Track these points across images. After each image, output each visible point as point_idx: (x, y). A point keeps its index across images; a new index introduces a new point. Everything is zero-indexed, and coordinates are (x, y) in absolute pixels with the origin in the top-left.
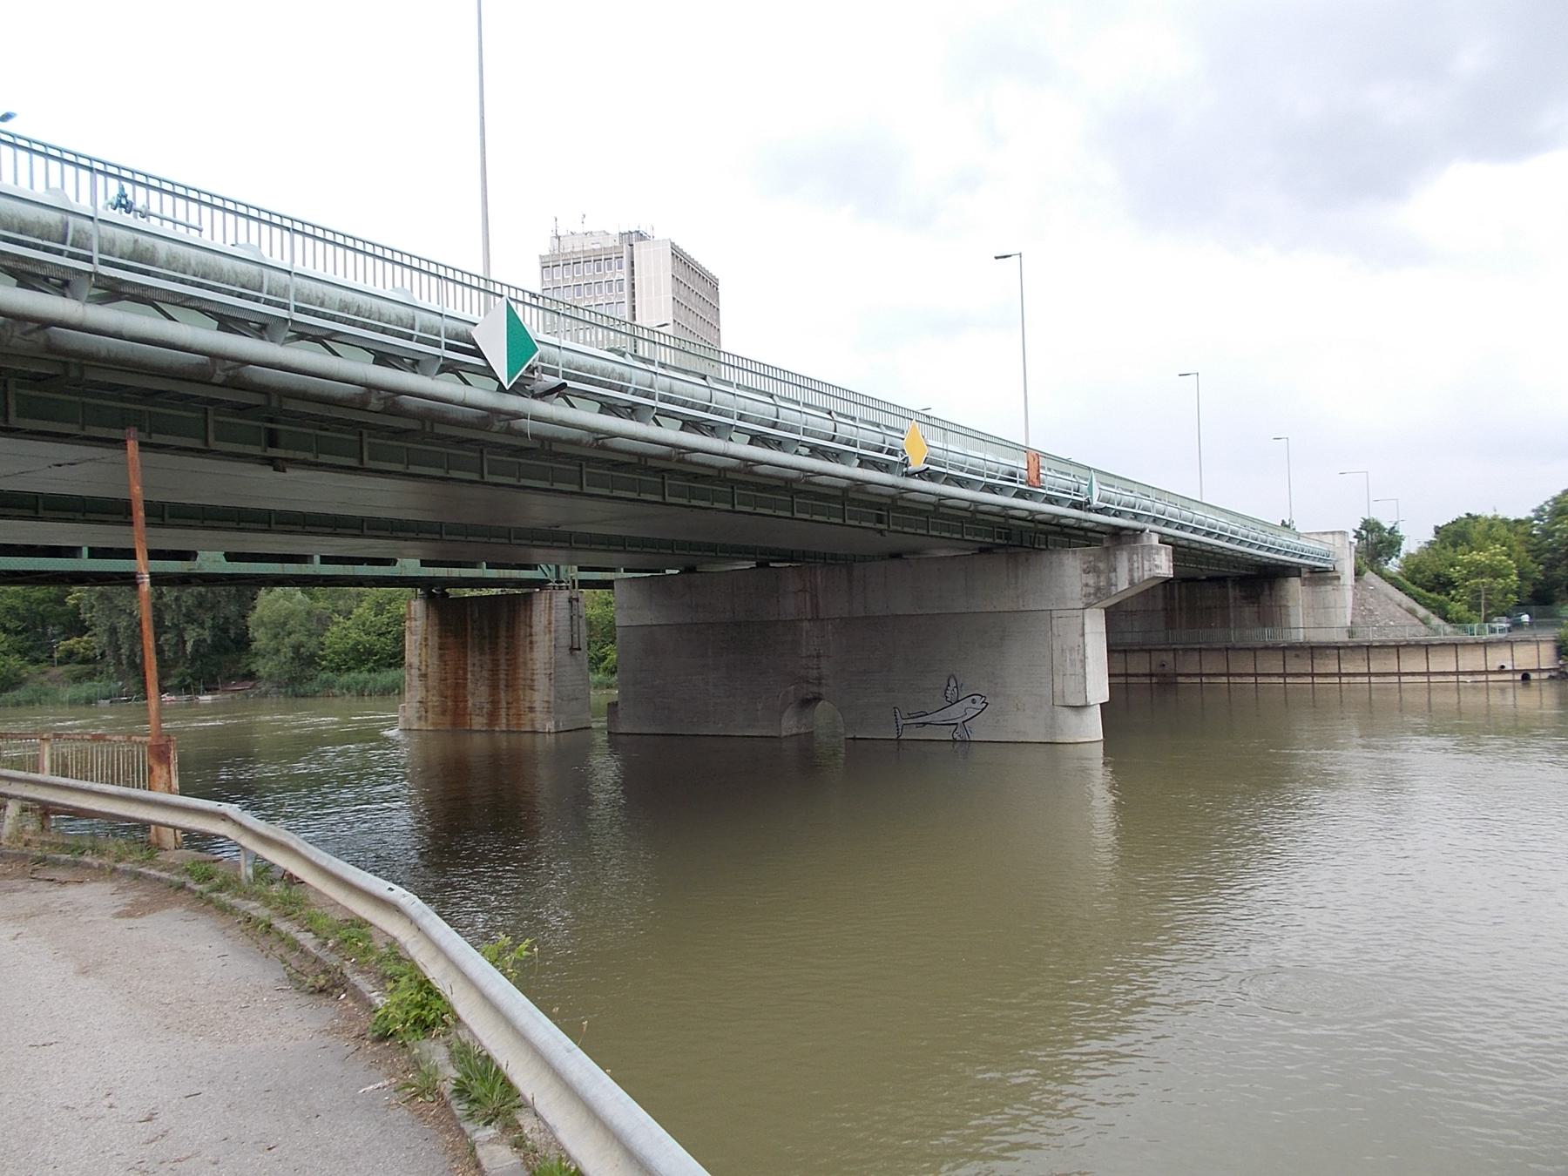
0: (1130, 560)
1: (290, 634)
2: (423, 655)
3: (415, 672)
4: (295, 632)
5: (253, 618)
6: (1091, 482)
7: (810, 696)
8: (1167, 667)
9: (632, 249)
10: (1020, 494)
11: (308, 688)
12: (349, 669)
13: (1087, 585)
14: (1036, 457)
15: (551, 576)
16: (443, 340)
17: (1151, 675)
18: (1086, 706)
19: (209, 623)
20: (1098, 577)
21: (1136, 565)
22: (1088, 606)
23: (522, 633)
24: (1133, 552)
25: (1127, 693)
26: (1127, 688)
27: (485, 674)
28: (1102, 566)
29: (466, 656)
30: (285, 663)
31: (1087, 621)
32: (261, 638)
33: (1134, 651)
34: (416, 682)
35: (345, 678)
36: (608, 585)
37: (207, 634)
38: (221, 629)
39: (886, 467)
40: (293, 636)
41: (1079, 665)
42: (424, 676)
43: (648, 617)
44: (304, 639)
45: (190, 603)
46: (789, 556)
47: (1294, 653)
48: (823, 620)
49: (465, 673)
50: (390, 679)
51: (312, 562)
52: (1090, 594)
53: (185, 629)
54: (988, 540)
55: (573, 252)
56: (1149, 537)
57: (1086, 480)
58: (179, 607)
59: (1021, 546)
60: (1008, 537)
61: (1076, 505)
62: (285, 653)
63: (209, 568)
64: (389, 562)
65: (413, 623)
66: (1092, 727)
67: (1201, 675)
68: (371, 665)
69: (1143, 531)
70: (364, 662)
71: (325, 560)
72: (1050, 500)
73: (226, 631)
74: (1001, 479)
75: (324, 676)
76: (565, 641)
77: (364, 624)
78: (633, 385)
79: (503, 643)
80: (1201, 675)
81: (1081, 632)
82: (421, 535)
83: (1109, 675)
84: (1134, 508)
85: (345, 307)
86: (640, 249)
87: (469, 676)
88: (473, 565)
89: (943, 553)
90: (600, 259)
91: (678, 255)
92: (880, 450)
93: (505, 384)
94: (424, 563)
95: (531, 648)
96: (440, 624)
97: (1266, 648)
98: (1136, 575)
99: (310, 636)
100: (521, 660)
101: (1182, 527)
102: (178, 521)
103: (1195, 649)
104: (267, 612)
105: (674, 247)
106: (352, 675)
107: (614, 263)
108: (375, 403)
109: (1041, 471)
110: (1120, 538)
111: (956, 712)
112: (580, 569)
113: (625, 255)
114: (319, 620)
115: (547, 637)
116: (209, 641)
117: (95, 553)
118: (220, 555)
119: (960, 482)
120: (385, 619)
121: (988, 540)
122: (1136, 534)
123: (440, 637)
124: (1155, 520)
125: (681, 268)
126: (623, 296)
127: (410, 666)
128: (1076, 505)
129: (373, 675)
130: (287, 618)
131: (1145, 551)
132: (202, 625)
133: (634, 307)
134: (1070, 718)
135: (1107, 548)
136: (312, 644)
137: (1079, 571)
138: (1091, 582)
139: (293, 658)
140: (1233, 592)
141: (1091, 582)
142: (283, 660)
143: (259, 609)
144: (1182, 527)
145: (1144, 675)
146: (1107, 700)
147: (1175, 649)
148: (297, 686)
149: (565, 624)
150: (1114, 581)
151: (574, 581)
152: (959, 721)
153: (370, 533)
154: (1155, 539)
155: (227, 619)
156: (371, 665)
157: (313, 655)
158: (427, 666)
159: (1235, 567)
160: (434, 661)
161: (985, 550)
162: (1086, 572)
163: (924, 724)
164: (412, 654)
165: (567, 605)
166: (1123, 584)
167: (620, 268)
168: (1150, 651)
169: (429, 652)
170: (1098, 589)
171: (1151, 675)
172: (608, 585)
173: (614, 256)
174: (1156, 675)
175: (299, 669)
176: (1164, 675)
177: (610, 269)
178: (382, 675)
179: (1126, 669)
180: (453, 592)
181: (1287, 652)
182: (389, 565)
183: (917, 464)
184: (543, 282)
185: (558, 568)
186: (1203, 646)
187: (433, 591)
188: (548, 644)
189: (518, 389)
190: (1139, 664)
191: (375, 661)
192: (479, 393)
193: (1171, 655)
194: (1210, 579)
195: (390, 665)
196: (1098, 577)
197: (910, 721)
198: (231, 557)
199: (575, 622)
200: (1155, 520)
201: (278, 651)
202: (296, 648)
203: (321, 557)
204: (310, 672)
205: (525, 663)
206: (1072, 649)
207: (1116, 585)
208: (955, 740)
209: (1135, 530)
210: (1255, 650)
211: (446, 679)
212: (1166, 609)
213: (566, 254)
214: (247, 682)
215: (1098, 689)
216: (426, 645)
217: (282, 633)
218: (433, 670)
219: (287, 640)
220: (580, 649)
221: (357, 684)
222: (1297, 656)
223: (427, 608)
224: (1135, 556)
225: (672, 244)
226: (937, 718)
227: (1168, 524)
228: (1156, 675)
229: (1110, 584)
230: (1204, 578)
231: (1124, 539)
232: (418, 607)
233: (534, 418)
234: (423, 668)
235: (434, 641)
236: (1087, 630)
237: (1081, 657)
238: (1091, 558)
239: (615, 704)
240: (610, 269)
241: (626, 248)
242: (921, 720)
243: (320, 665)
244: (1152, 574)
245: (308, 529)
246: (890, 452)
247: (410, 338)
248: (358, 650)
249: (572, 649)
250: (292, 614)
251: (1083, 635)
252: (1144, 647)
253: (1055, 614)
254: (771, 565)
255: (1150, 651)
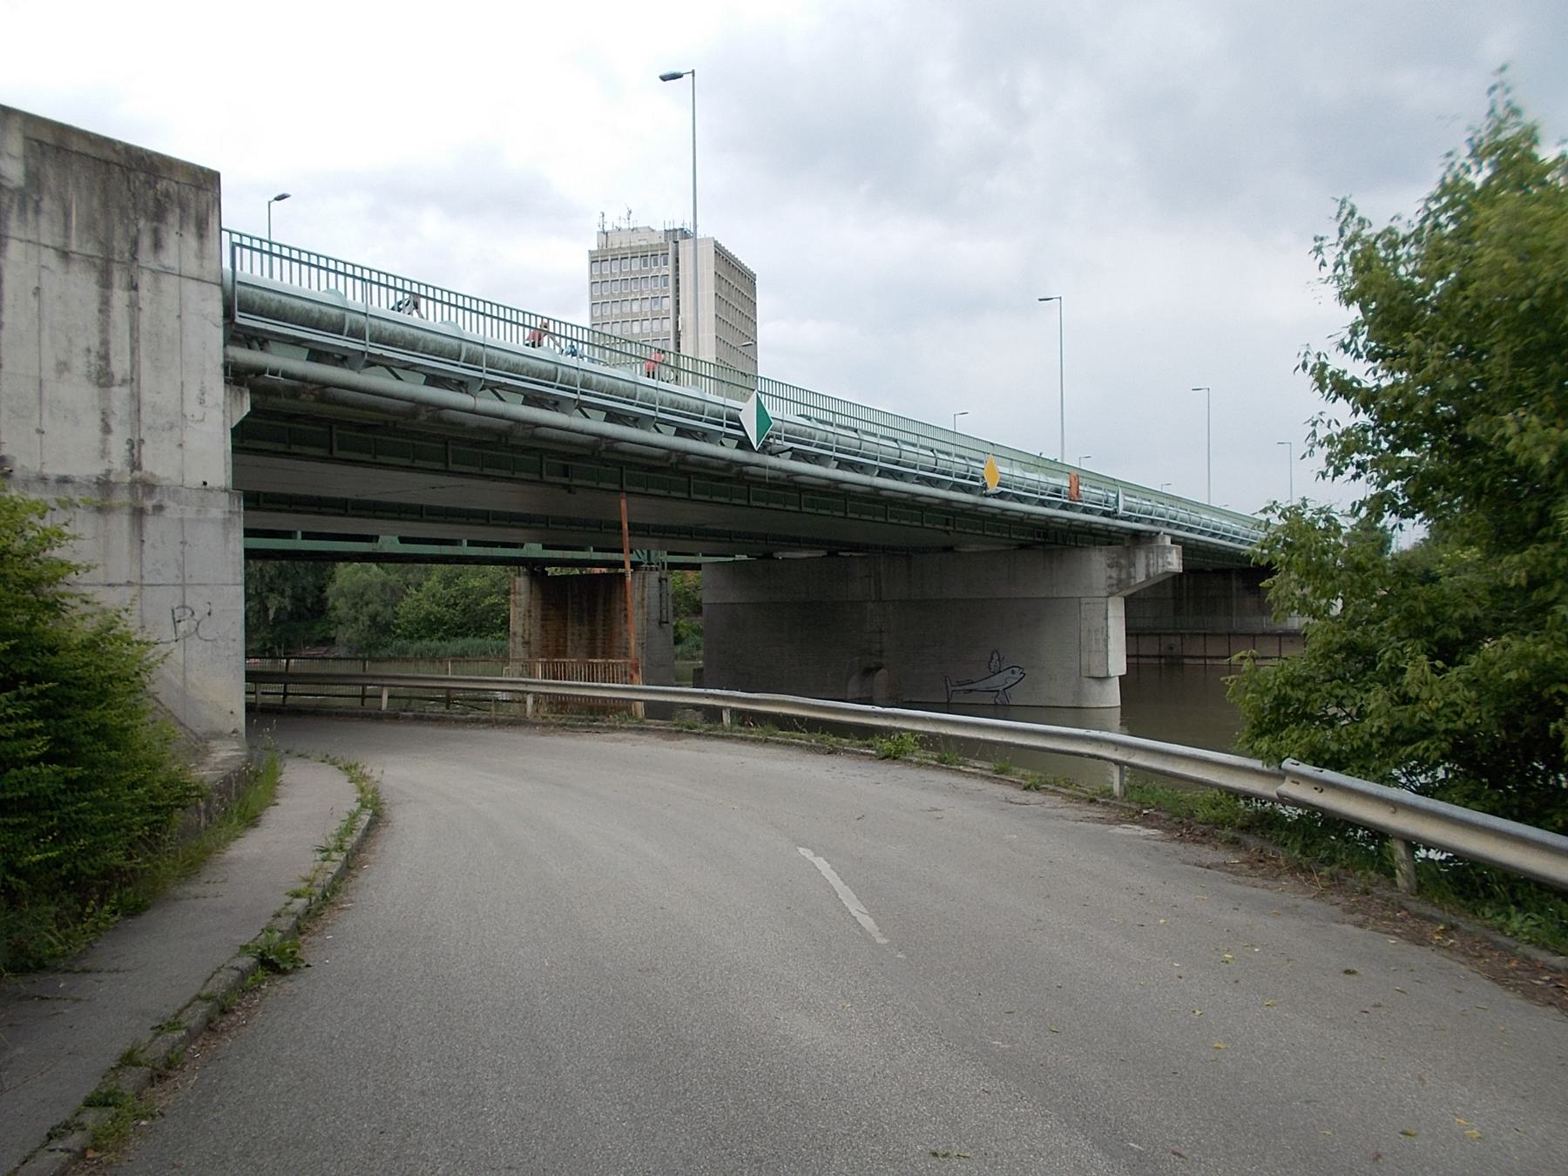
0: (1147, 557)
1: (367, 604)
2: (527, 627)
3: (519, 640)
4: (371, 602)
5: (331, 590)
6: (1118, 496)
7: (873, 666)
8: (1175, 650)
9: (677, 246)
10: (1064, 507)
11: (384, 653)
12: (421, 638)
13: (1110, 577)
14: (1077, 476)
15: (644, 558)
16: (725, 422)
17: (1160, 657)
18: (1108, 677)
19: (289, 592)
20: (1120, 571)
21: (1151, 562)
22: (1111, 594)
23: (618, 607)
24: (1150, 551)
25: (1138, 673)
26: (1138, 668)
27: (584, 642)
28: (1123, 561)
29: (566, 626)
30: (363, 631)
31: (1110, 608)
32: (341, 607)
33: (1145, 635)
34: (520, 648)
35: (418, 645)
36: (697, 567)
37: (287, 602)
38: (298, 599)
39: (968, 490)
40: (370, 606)
41: (1102, 643)
42: (527, 643)
43: (732, 597)
44: (381, 609)
45: (272, 573)
46: (856, 547)
47: (1288, 639)
48: (885, 601)
49: (566, 641)
50: (459, 647)
51: (296, 538)
52: (1113, 585)
53: (267, 597)
54: (1029, 538)
55: (620, 248)
56: (1163, 538)
57: (1113, 492)
58: (262, 577)
59: (1056, 543)
60: (1046, 536)
61: (1105, 514)
62: (363, 621)
63: (386, 550)
64: (520, 545)
65: (518, 597)
66: (1112, 695)
67: (1205, 657)
68: (440, 634)
69: (1158, 533)
70: (434, 631)
71: (471, 543)
72: (1086, 511)
73: (303, 600)
74: (1049, 495)
75: (399, 643)
76: (655, 615)
77: (434, 596)
78: (816, 441)
79: (600, 617)
80: (1205, 657)
81: (1104, 615)
82: (533, 525)
83: (1127, 656)
84: (1150, 514)
85: (672, 404)
86: (686, 248)
87: (569, 643)
88: (582, 549)
89: (973, 548)
90: (647, 255)
91: (721, 254)
92: (964, 477)
93: (755, 445)
94: (545, 547)
95: (626, 622)
96: (542, 599)
97: (1264, 634)
98: (1151, 570)
99: (385, 606)
100: (617, 630)
101: (1190, 530)
102: (271, 506)
103: (1198, 634)
104: (347, 584)
105: (717, 245)
106: (424, 642)
107: (660, 260)
108: (674, 459)
109: (1081, 488)
110: (1139, 540)
111: (997, 681)
112: (669, 554)
113: (670, 251)
114: (393, 591)
115: (641, 611)
116: (289, 609)
117: (307, 536)
118: (396, 539)
119: (1020, 499)
120: (453, 590)
121: (1029, 538)
122: (1151, 537)
123: (542, 610)
124: (1168, 524)
125: (724, 266)
126: (668, 291)
127: (514, 634)
128: (1105, 514)
129: (443, 643)
130: (365, 588)
131: (1160, 550)
132: (282, 594)
133: (678, 301)
134: (1095, 687)
135: (1128, 547)
136: (388, 613)
137: (1104, 565)
138: (1114, 575)
139: (370, 626)
140: (1236, 584)
141: (1114, 575)
142: (362, 627)
143: (339, 581)
144: (1190, 530)
145: (1154, 656)
146: (1124, 673)
147: (1182, 634)
148: (373, 652)
149: (655, 601)
150: (1133, 574)
151: (663, 564)
152: (1001, 689)
153: (353, 512)
154: (1168, 540)
155: (304, 589)
156: (440, 634)
157: (388, 624)
158: (530, 635)
159: (1238, 561)
160: (537, 630)
161: (1023, 547)
162: (1110, 566)
163: (971, 690)
164: (516, 625)
165: (656, 583)
166: (1140, 577)
167: (666, 264)
168: (1159, 635)
169: (532, 622)
170: (1120, 581)
171: (1160, 657)
172: (697, 567)
173: (660, 252)
174: (1165, 657)
175: (375, 637)
176: (1172, 657)
177: (656, 264)
178: (452, 643)
179: (1138, 650)
180: (550, 571)
181: (1283, 639)
182: (371, 541)
183: (993, 488)
184: (591, 276)
185: (649, 552)
186: (1208, 632)
187: (534, 568)
188: (641, 618)
189: (765, 449)
190: (1149, 647)
191: (445, 631)
192: (729, 451)
193: (1179, 639)
194: (1216, 571)
195: (456, 635)
196: (1120, 571)
197: (958, 688)
198: (403, 540)
199: (664, 599)
200: (1168, 524)
201: (356, 619)
202: (373, 618)
203: (468, 541)
204: (384, 639)
205: (621, 635)
206: (1096, 630)
207: (1134, 578)
208: (996, 704)
209: (1151, 532)
210: (1254, 635)
211: (547, 647)
212: (1175, 598)
213: (614, 250)
214: (319, 648)
215: (1118, 665)
216: (530, 616)
217: (360, 603)
218: (536, 638)
219: (365, 609)
220: (667, 623)
221: (429, 650)
222: (1291, 641)
223: (531, 584)
224: (1151, 555)
225: (716, 242)
226: (981, 686)
227: (1179, 527)
228: (1165, 657)
229: (1130, 577)
230: (1210, 570)
231: (1142, 540)
232: (521, 583)
233: (770, 468)
234: (526, 636)
235: (537, 613)
236: (1110, 615)
237: (1104, 637)
238: (1115, 555)
239: (701, 670)
240: (656, 264)
241: (671, 245)
242: (968, 687)
243: (394, 633)
244: (1165, 569)
245: (449, 519)
246: (972, 479)
247: (700, 420)
248: (430, 620)
249: (661, 622)
250: (369, 585)
251: (1106, 619)
252: (1155, 632)
253: (1083, 601)
254: (841, 554)
255: (1159, 635)
